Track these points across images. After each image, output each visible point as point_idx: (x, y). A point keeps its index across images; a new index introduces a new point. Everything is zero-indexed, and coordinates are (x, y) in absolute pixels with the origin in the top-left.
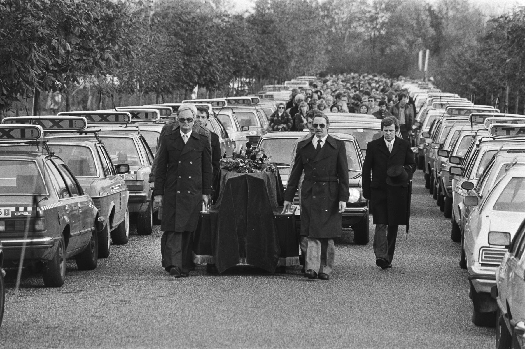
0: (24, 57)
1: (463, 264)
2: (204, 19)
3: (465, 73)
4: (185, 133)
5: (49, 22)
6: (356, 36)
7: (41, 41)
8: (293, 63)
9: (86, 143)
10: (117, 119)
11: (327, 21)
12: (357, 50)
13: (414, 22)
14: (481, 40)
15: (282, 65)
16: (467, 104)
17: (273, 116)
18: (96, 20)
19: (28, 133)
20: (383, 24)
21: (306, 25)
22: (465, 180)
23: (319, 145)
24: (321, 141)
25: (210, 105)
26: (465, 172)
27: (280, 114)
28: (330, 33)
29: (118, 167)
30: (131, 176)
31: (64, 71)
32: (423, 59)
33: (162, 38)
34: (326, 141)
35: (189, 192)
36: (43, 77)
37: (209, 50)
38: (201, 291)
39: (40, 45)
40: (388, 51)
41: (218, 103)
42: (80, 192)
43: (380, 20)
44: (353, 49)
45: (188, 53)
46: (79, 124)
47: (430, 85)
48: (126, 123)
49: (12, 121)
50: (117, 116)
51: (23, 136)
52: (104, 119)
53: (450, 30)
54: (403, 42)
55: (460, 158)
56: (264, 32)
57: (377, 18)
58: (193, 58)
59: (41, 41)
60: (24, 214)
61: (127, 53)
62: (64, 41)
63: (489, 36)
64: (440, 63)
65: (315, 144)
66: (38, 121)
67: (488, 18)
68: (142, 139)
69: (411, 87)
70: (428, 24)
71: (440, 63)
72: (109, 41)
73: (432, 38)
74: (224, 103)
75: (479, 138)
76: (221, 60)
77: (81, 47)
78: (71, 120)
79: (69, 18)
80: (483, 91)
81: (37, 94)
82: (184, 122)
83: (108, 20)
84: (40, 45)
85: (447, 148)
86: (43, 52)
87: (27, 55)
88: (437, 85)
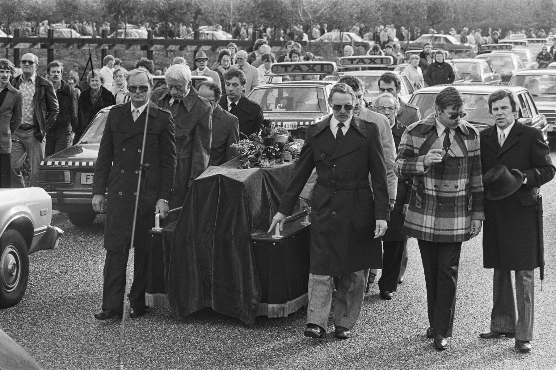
4: (137, 107)
17: (540, 54)
23: (340, 131)
24: (344, 125)
27: (544, 54)
34: (350, 125)
38: (547, 257)
60: (304, 126)
65: (334, 130)
82: (135, 92)
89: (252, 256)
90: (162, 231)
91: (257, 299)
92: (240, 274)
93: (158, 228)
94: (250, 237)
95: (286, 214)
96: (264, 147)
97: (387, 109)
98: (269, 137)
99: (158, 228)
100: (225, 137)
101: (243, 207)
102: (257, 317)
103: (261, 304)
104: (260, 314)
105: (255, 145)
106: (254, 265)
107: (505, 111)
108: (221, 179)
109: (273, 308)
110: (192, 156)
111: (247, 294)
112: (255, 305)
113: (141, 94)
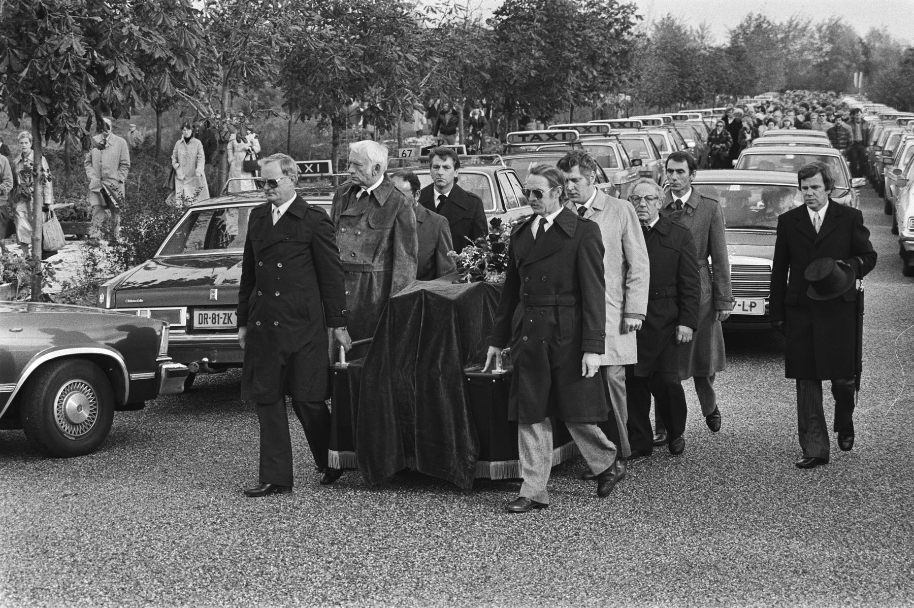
0: (562, 81)
1: (895, 231)
2: (694, 50)
3: (890, 89)
5: (581, 55)
6: (806, 62)
7: (575, 68)
8: (760, 83)
9: (609, 144)
10: (632, 125)
11: (785, 51)
12: (808, 72)
13: (850, 52)
14: (901, 64)
15: (752, 84)
16: (893, 112)
18: (615, 53)
19: (568, 137)
20: (827, 53)
21: (769, 54)
22: (895, 168)
24: (547, 222)
25: (700, 114)
26: (894, 162)
28: (787, 59)
29: (633, 161)
30: (643, 168)
31: (591, 91)
32: (858, 79)
33: (663, 65)
35: (276, 324)
36: (576, 96)
37: (697, 73)
39: (574, 72)
40: (831, 73)
41: (706, 113)
42: (607, 181)
43: (824, 50)
44: (805, 72)
45: (682, 76)
46: (604, 130)
47: (864, 99)
48: (639, 128)
49: (555, 128)
50: (632, 123)
51: (564, 139)
52: (622, 125)
53: (876, 57)
54: (841, 66)
55: (890, 152)
56: (738, 60)
57: (821, 49)
58: (686, 80)
59: (575, 68)
61: (639, 77)
62: (591, 69)
63: (907, 61)
64: (871, 82)
66: (575, 128)
67: (904, 49)
68: (651, 140)
69: (851, 101)
70: (860, 53)
71: (871, 82)
72: (624, 68)
73: (864, 63)
74: (709, 113)
75: (904, 137)
76: (706, 81)
77: (605, 73)
78: (598, 127)
79: (595, 52)
80: (903, 102)
81: (572, 108)
83: (624, 53)
84: (574, 72)
85: (880, 144)
86: (577, 77)
87: (564, 79)
88: (870, 98)
89: (466, 397)
90: (349, 367)
91: (474, 455)
92: (452, 421)
93: (344, 363)
94: (463, 372)
95: (501, 346)
96: (492, 255)
97: (643, 200)
98: (500, 241)
99: (344, 363)
100: (433, 246)
101: (454, 333)
102: (475, 479)
103: (479, 463)
104: (479, 475)
105: (482, 254)
106: (468, 410)
107: (817, 192)
108: (426, 297)
109: (496, 467)
110: (392, 271)
111: (461, 448)
112: (472, 463)
113: (271, 191)
